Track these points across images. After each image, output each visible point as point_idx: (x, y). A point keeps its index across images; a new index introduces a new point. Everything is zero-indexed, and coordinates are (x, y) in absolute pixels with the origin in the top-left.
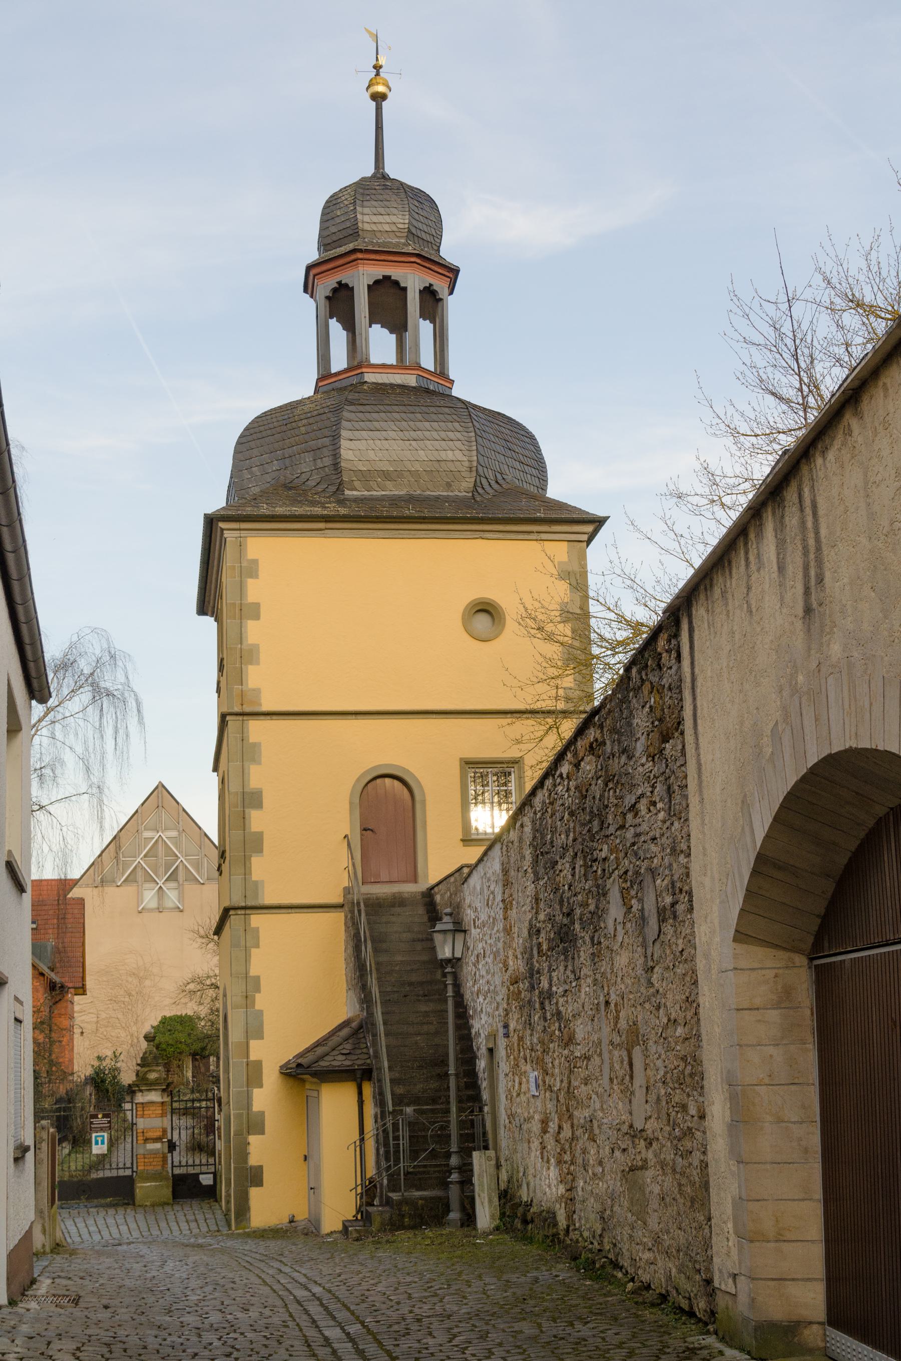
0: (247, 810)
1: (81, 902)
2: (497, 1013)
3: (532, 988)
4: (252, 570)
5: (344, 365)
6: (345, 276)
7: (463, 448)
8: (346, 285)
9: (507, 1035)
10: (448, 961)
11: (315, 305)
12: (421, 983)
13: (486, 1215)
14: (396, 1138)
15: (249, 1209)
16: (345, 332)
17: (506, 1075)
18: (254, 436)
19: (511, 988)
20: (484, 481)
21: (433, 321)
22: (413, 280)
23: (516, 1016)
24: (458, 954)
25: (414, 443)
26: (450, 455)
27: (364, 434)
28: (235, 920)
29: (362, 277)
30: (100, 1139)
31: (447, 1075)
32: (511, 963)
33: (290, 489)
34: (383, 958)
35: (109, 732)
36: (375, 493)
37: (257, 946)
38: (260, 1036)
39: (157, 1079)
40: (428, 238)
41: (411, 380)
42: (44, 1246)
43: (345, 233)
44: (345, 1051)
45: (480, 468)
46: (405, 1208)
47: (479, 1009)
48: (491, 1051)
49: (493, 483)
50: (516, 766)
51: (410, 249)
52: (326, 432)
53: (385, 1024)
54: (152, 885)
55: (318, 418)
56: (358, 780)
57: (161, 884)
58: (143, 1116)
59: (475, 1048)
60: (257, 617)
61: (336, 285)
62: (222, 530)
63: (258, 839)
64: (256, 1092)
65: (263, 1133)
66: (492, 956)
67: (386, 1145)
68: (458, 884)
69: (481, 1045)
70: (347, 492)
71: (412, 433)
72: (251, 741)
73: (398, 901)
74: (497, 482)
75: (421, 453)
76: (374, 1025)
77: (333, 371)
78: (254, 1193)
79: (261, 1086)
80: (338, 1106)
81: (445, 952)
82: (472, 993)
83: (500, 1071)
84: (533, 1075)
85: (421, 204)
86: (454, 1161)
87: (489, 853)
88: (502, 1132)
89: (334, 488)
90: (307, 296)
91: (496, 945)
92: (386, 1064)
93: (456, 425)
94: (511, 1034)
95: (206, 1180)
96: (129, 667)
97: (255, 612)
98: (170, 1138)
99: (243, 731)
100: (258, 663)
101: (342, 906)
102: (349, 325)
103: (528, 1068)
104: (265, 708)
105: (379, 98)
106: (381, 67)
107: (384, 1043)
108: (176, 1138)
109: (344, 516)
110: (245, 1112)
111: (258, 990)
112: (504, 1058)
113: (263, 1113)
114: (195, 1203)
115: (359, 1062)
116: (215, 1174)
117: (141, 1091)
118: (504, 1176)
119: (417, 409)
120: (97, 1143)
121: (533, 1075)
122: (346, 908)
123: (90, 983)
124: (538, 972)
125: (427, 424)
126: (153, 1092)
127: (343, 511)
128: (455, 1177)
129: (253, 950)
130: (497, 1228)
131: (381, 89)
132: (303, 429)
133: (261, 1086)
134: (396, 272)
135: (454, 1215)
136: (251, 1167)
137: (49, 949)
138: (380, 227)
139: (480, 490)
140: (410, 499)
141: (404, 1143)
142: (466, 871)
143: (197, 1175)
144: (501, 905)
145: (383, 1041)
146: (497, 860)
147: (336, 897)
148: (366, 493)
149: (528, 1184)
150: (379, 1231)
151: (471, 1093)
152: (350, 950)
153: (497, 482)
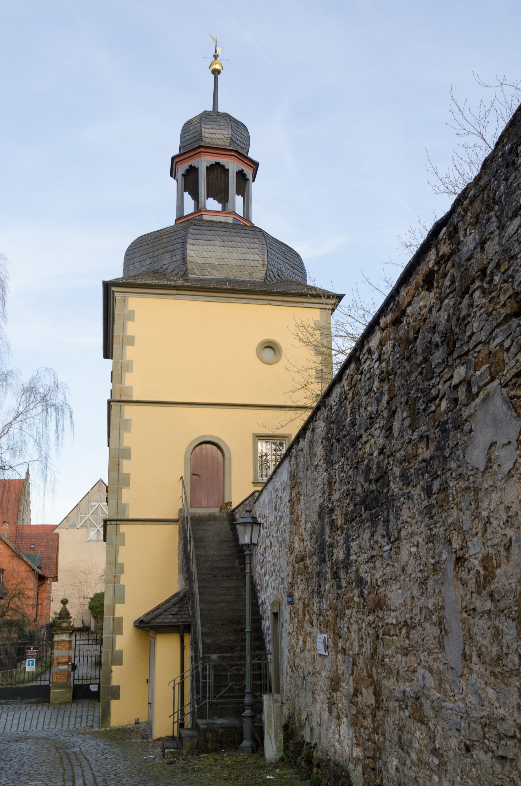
0: (121, 460)
2: (282, 586)
3: (323, 561)
4: (131, 316)
5: (192, 210)
6: (193, 162)
7: (259, 253)
8: (194, 167)
9: (291, 603)
10: (248, 546)
12: (225, 569)
13: (272, 748)
14: (204, 677)
15: (110, 714)
16: (193, 201)
17: (290, 634)
18: (137, 246)
19: (297, 566)
20: (271, 274)
21: (243, 196)
22: (233, 166)
23: (301, 587)
24: (254, 541)
25: (230, 249)
26: (252, 257)
27: (201, 242)
28: (110, 528)
29: (203, 162)
30: (31, 662)
31: (243, 630)
32: (297, 546)
33: (156, 273)
34: (202, 552)
35: (52, 426)
36: (207, 277)
37: (123, 544)
38: (122, 600)
39: (67, 627)
40: (242, 145)
41: (230, 220)
43: (194, 139)
44: (173, 613)
45: (269, 266)
46: (209, 735)
47: (265, 585)
48: (276, 615)
49: (276, 276)
50: (286, 439)
51: (231, 148)
52: (179, 241)
53: (200, 594)
54: (94, 528)
55: (174, 233)
56: (190, 444)
57: (98, 528)
58: (57, 649)
59: (261, 612)
60: (132, 344)
61: (188, 167)
62: (114, 292)
63: (127, 477)
64: (118, 638)
65: (121, 664)
66: (278, 546)
67: (197, 681)
68: (251, 504)
69: (267, 610)
70: (190, 276)
71: (230, 243)
72: (125, 418)
73: (212, 518)
74: (279, 276)
75: (235, 254)
76: (193, 595)
80: (168, 650)
81: (245, 539)
82: (260, 575)
83: (284, 630)
84: (321, 638)
85: (239, 128)
86: (248, 699)
87: (278, 471)
88: (284, 678)
89: (182, 273)
90: (172, 179)
91: (282, 535)
92: (199, 622)
93: (256, 240)
94: (297, 601)
95: (94, 688)
96: (67, 393)
97: (131, 341)
98: (73, 662)
99: (120, 412)
100: (132, 372)
101: (177, 521)
102: (195, 196)
103: (315, 629)
104: (135, 398)
105: (216, 72)
106: (218, 56)
107: (198, 608)
108: (77, 662)
110: (110, 650)
111: (122, 572)
112: (288, 620)
113: (121, 652)
114: (86, 702)
115: (182, 620)
116: (99, 685)
117: (57, 634)
118: (286, 712)
119: (233, 230)
120: (29, 665)
121: (321, 638)
123: (60, 575)
124: (331, 546)
125: (239, 239)
126: (64, 635)
127: (186, 284)
128: (247, 712)
129: (121, 547)
130: (282, 759)
131: (217, 67)
132: (165, 240)
134: (224, 161)
135: (246, 743)
136: (112, 687)
137: (38, 557)
138: (214, 136)
139: (269, 278)
140: (228, 280)
141: (210, 681)
142: (257, 494)
143: (88, 685)
144: (288, 504)
145: (198, 606)
146: (286, 472)
147: (174, 516)
148: (201, 277)
149: (312, 729)
150: (188, 753)
151: (258, 643)
152: (181, 548)
153: (279, 276)
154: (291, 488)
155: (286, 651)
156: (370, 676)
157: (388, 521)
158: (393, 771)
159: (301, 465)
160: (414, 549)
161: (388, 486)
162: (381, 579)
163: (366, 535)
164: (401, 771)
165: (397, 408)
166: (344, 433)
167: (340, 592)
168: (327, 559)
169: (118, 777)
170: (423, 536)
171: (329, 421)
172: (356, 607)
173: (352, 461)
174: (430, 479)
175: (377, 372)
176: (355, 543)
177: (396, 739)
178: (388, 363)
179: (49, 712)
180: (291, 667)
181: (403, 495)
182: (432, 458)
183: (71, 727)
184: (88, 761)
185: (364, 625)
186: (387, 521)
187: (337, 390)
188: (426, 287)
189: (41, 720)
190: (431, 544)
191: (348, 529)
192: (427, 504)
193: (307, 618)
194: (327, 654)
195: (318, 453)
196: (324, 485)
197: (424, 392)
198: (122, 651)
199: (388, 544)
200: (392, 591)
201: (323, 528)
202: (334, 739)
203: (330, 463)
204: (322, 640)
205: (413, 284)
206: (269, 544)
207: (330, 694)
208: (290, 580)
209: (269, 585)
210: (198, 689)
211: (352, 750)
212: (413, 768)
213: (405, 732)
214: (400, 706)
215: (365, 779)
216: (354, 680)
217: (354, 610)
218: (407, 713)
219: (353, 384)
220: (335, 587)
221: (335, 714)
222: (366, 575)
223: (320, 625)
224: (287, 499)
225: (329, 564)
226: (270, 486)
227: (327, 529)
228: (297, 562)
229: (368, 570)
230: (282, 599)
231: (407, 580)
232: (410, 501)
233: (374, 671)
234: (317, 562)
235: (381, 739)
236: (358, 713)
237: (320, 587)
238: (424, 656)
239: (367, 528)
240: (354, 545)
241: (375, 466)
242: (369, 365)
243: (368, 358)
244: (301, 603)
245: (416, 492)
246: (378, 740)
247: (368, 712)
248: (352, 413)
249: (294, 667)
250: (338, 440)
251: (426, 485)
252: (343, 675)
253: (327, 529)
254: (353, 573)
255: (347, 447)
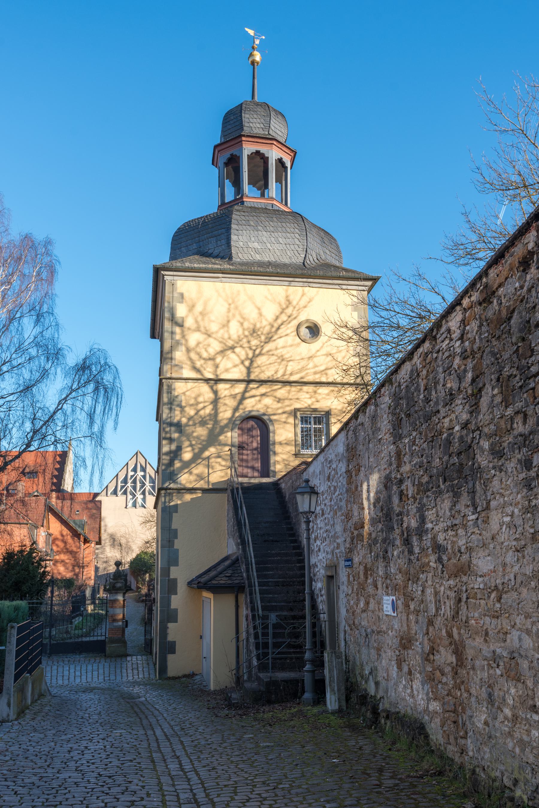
1: (100, 502)
8: (236, 156)
11: (217, 171)
23: (362, 552)
24: (312, 509)
38: (176, 564)
42: (8, 715)
47: (316, 549)
48: (330, 578)
49: (315, 259)
61: (229, 156)
62: (163, 275)
65: (177, 622)
66: (332, 513)
77: (226, 201)
78: (170, 657)
79: (176, 594)
109: (232, 270)
111: (176, 537)
112: (346, 583)
121: (387, 601)
122: (229, 491)
124: (400, 514)
128: (308, 667)
133: (176, 594)
134: (263, 149)
135: (307, 695)
136: (169, 642)
140: (270, 264)
149: (377, 684)
152: (231, 514)
154: (348, 460)
155: (343, 612)
156: (450, 635)
157: (474, 492)
158: (480, 725)
159: (361, 439)
160: (507, 519)
161: (474, 459)
162: (464, 547)
163: (447, 504)
164: (491, 725)
165: (484, 385)
166: (416, 409)
167: (412, 557)
168: (396, 527)
169: (193, 726)
170: (520, 507)
171: (396, 397)
172: (432, 572)
173: (426, 435)
174: (530, 453)
175: (458, 350)
176: (430, 512)
177: (484, 695)
178: (473, 342)
179: (107, 665)
180: (349, 626)
181: (494, 468)
182: (531, 433)
183: (130, 678)
184: (158, 710)
185: (442, 588)
186: (472, 492)
187: (407, 367)
188: (521, 268)
189: (101, 671)
190: (529, 515)
191: (421, 499)
192: (525, 476)
193: (370, 581)
194: (395, 615)
195: (383, 429)
196: (391, 457)
197: (522, 369)
198: (177, 609)
199: (473, 514)
200: (479, 558)
201: (390, 497)
202: (405, 694)
203: (397, 437)
204: (390, 602)
205: (507, 266)
206: (321, 512)
207: (400, 651)
208: (348, 546)
209: (322, 550)
210: (262, 646)
211: (428, 703)
212: (506, 723)
213: (496, 688)
214: (489, 665)
215: (444, 731)
216: (429, 639)
217: (431, 574)
218: (498, 672)
219: (427, 361)
220: (406, 553)
221: (405, 669)
222: (445, 542)
223: (387, 588)
224: (344, 470)
225: (397, 531)
226: (321, 458)
227: (396, 500)
228: (356, 529)
229: (447, 537)
230: (338, 563)
231: (498, 547)
232: (503, 473)
233: (455, 630)
234: (382, 529)
235: (465, 695)
236: (434, 670)
237: (387, 552)
238: (519, 620)
239: (446, 498)
240: (430, 515)
241: (456, 440)
242: (448, 344)
243: (446, 337)
244: (362, 567)
245: (511, 465)
246: (461, 695)
247: (448, 669)
248: (426, 389)
249: (353, 626)
250: (408, 416)
251: (524, 458)
252: (416, 634)
253: (396, 500)
254: (430, 540)
255: (420, 422)
